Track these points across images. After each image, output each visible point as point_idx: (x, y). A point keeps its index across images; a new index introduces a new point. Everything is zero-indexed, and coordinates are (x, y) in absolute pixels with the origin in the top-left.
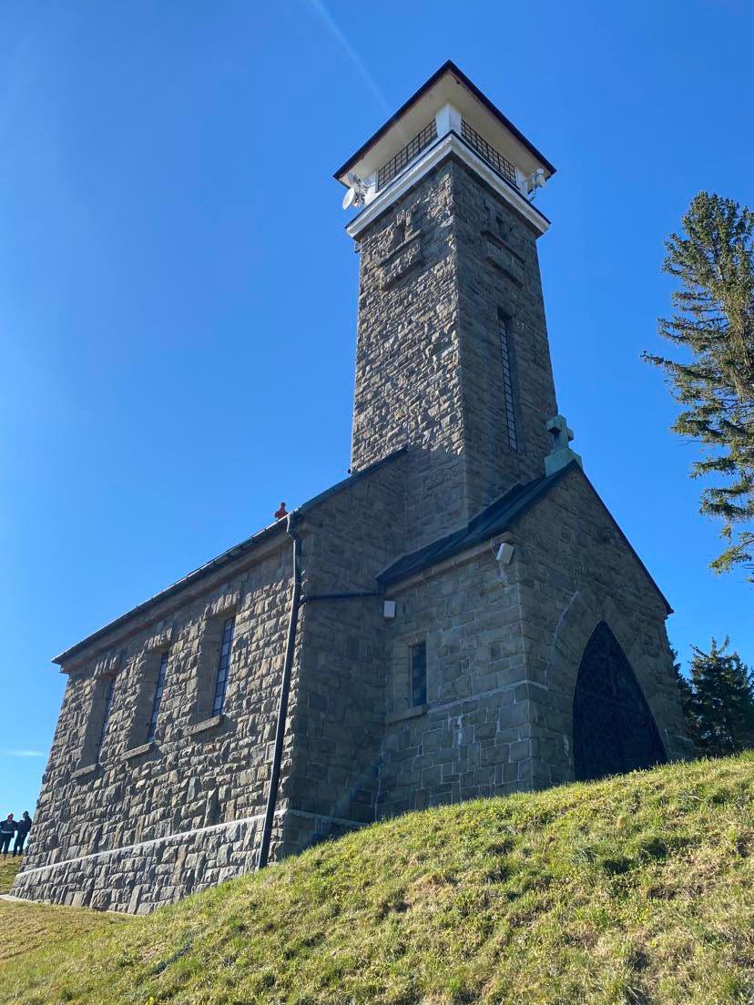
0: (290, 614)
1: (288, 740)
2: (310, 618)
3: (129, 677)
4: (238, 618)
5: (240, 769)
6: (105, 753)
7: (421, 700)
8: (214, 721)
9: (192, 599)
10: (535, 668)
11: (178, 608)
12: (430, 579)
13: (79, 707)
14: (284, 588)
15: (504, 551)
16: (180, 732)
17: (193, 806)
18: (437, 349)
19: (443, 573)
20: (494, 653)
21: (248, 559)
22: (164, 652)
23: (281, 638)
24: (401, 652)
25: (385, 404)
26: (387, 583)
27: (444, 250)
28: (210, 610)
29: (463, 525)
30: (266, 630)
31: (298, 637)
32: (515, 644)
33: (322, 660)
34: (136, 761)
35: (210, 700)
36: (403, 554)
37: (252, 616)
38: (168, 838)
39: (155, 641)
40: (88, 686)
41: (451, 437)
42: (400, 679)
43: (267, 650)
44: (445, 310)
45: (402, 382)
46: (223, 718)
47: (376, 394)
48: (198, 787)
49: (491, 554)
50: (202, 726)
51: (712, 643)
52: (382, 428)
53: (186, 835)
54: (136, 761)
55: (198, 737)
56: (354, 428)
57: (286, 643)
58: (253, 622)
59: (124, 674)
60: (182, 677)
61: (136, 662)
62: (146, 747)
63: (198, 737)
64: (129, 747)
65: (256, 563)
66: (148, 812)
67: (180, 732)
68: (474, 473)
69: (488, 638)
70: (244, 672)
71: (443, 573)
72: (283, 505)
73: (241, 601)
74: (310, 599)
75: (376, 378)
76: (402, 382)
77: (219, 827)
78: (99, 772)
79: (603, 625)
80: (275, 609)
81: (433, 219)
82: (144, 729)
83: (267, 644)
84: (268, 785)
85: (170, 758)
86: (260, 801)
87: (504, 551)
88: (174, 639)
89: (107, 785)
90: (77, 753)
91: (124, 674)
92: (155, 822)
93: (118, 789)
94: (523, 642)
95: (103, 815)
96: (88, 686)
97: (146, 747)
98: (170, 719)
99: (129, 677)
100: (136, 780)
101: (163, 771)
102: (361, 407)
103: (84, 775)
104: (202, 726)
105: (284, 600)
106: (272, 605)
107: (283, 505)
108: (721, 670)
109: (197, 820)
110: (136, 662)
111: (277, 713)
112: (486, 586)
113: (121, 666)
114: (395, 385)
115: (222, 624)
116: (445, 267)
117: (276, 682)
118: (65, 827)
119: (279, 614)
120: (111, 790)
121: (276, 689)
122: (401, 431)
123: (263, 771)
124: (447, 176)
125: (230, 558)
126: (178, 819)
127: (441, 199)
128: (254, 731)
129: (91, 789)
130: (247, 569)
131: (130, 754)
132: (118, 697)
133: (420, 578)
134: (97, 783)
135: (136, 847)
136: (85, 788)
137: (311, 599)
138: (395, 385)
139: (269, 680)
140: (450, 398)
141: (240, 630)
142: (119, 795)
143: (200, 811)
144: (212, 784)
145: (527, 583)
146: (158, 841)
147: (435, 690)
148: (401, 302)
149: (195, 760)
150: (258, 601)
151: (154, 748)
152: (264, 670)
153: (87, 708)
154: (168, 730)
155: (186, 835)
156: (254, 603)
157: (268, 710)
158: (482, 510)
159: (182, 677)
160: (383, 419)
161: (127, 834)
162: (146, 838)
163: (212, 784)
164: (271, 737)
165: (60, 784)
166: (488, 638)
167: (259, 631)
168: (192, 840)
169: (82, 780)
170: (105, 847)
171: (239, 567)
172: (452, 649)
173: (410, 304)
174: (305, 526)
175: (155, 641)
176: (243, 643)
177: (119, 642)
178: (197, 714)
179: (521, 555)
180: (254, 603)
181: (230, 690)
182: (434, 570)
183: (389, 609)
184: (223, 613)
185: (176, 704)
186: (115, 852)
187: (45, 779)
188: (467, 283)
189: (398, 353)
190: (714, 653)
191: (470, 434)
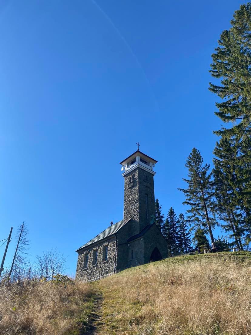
0: (116, 247)
1: (116, 263)
2: (118, 248)
3: (91, 254)
4: (108, 247)
5: (110, 267)
6: (88, 266)
7: (133, 258)
8: (106, 261)
9: (101, 243)
10: (145, 254)
11: (98, 244)
12: (134, 242)
13: (82, 259)
14: (115, 243)
15: (142, 239)
16: (101, 263)
17: (104, 272)
18: (136, 203)
19: (135, 241)
20: (141, 252)
21: (109, 238)
22: (97, 251)
23: (115, 250)
24: (130, 251)
25: (128, 210)
26: (129, 241)
27: (136, 185)
28: (104, 245)
29: (138, 233)
30: (112, 247)
31: (117, 250)
32: (143, 251)
33: (120, 253)
34: (93, 267)
35: (105, 258)
36: (131, 236)
37: (110, 247)
38: (100, 277)
39: (95, 249)
40: (83, 255)
41: (137, 219)
42: (130, 255)
43: (113, 252)
44: (137, 196)
45: (131, 207)
46: (107, 261)
47: (127, 208)
48: (104, 270)
49: (141, 239)
50: (104, 262)
51: (218, 237)
52: (128, 214)
53: (103, 276)
54: (93, 267)
55: (103, 263)
56: (124, 213)
57: (115, 251)
58: (110, 247)
59: (90, 254)
60: (100, 255)
61: (92, 252)
62: (96, 265)
63: (103, 263)
64: (93, 265)
65: (111, 239)
66: (97, 274)
67: (101, 263)
68: (140, 225)
69: (140, 250)
70: (110, 254)
71: (135, 241)
72: (112, 221)
73: (108, 244)
74: (118, 245)
75: (127, 205)
76: (131, 207)
77: (108, 275)
78: (87, 269)
79: (156, 248)
80: (113, 246)
81: (135, 178)
82: (94, 262)
83: (113, 251)
84: (114, 269)
85: (100, 266)
86: (113, 271)
87: (142, 239)
88: (98, 249)
89: (89, 271)
90: (83, 266)
91: (90, 254)
92: (98, 275)
93: (91, 271)
94: (144, 251)
95: (89, 275)
96: (83, 255)
97: (96, 265)
98: (99, 261)
99: (91, 254)
100: (94, 270)
101: (99, 268)
102: (125, 209)
103: (85, 270)
104: (104, 262)
105: (115, 245)
106: (113, 245)
107: (112, 221)
108: (221, 244)
109: (105, 274)
110: (92, 252)
111: (115, 260)
112: (140, 243)
113: (89, 252)
114: (130, 207)
115: (105, 248)
116: (137, 188)
117: (114, 256)
118: (82, 277)
119: (114, 247)
120: (90, 271)
121: (114, 257)
122: (131, 216)
123: (113, 267)
124: (137, 171)
125: (107, 238)
126: (102, 274)
127: (137, 175)
128: (111, 262)
129: (86, 272)
130: (109, 239)
131: (93, 266)
132: (89, 257)
133: (132, 241)
134: (87, 271)
135: (96, 279)
136: (85, 271)
137: (118, 245)
138: (130, 207)
139: (113, 255)
140: (137, 212)
141: (109, 248)
142: (92, 272)
143: (105, 273)
144: (106, 269)
145: (145, 243)
146: (99, 277)
147: (134, 257)
148: (131, 192)
149: (103, 266)
150: (111, 244)
151: (97, 265)
152: (112, 254)
153: (83, 259)
154: (99, 262)
155: (103, 276)
156: (110, 245)
157: (113, 260)
158: (141, 230)
159: (100, 255)
160: (128, 213)
161: (94, 277)
162: (97, 277)
163: (106, 269)
164: (114, 263)
165: (80, 271)
166: (140, 250)
167: (111, 249)
168: (104, 277)
169: (84, 270)
170: (90, 279)
171: (108, 239)
172: (136, 251)
173: (132, 193)
174: (117, 234)
175: (95, 249)
176: (109, 250)
177: (88, 248)
178: (104, 260)
179: (145, 239)
180: (110, 245)
181: (108, 257)
182: (135, 240)
183: (129, 245)
184: (106, 246)
185: (100, 258)
186: (92, 280)
187: (77, 271)
188: (140, 191)
189: (130, 202)
190: (219, 240)
191: (140, 218)
